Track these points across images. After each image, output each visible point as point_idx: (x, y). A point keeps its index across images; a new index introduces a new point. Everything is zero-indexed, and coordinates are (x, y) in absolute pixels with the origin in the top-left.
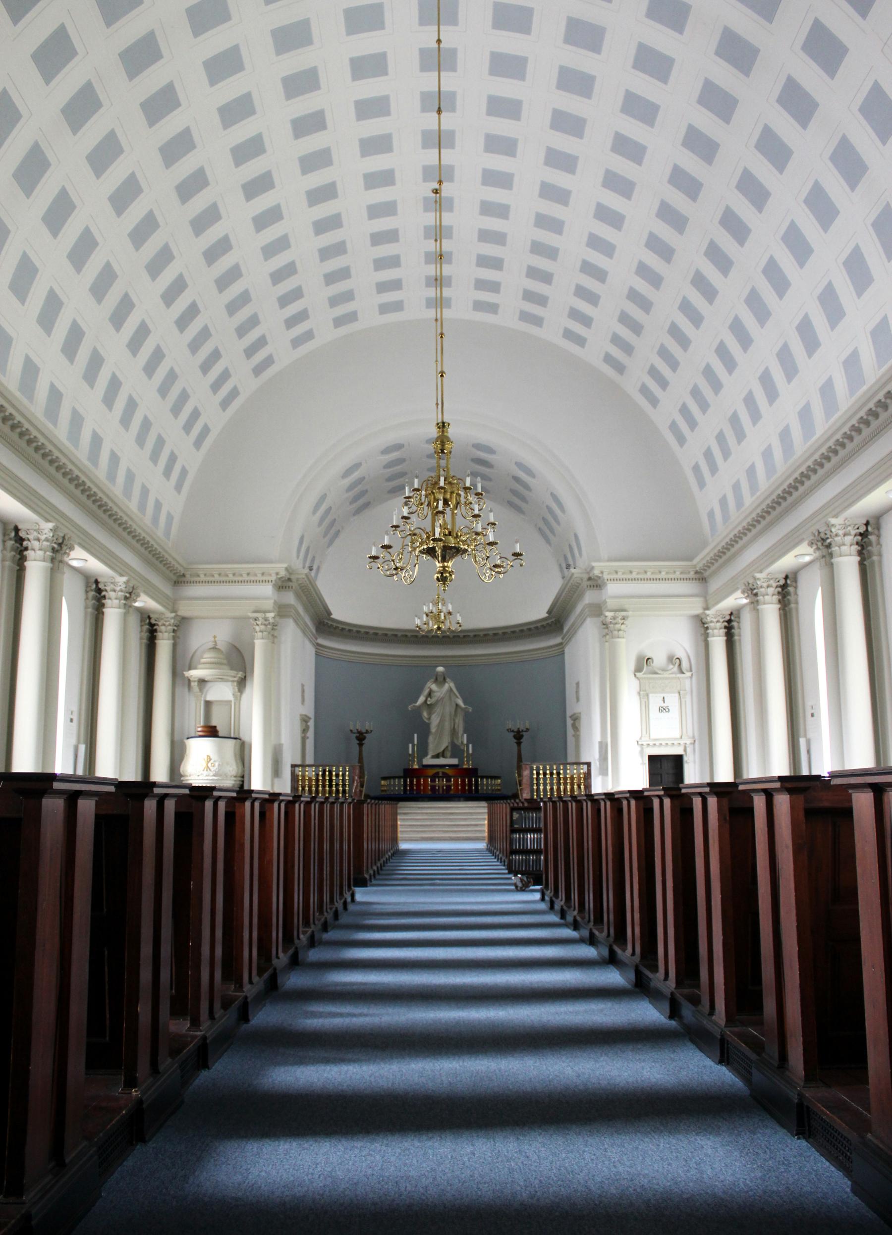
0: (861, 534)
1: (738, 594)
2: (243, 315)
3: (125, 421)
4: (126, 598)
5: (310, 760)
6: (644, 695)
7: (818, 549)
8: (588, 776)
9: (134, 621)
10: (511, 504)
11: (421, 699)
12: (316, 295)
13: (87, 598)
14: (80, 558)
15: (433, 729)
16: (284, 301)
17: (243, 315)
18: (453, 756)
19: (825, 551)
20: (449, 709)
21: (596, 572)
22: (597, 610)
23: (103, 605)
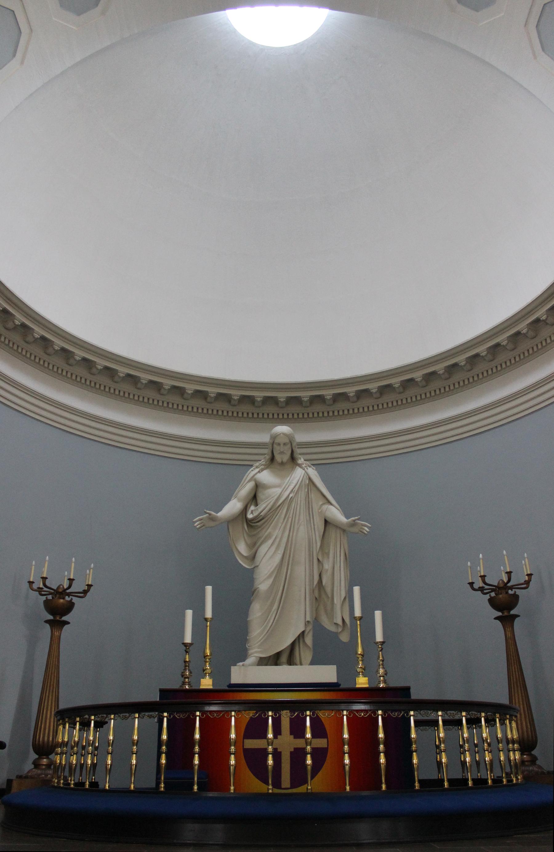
11: (233, 506)
15: (263, 584)
18: (317, 660)
20: (305, 533)
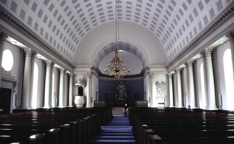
0: (212, 52)
1: (183, 65)
2: (84, 21)
3: (61, 38)
4: (64, 72)
5: (98, 99)
6: (157, 88)
7: (230, 37)
8: (147, 103)
9: (66, 76)
10: (134, 53)
11: (118, 88)
12: (98, 17)
13: (21, 54)
14: (56, 66)
15: (120, 93)
16: (92, 19)
17: (84, 21)
19: (203, 56)
21: (148, 67)
22: (149, 73)
23: (46, 67)
